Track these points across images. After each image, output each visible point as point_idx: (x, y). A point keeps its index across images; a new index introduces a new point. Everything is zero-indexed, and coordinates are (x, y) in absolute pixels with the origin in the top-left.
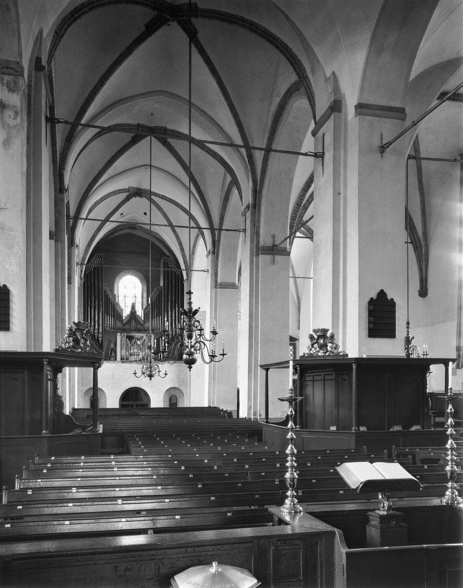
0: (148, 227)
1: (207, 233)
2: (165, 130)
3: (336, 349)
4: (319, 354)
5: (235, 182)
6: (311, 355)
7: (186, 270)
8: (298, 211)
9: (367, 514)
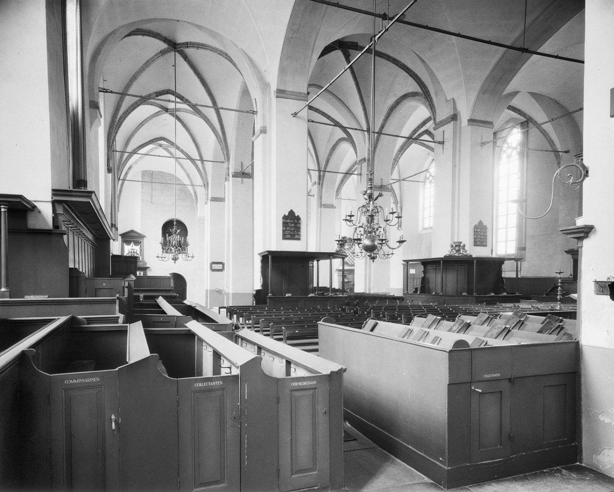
4: (456, 255)
6: (450, 256)
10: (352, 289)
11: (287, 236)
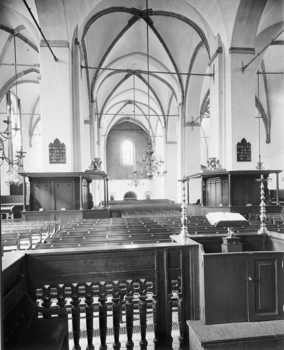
0: (133, 117)
1: (162, 118)
2: (141, 72)
3: (220, 167)
4: (212, 170)
5: (174, 93)
7: (153, 136)
8: (204, 105)
9: (222, 238)
10: (150, 198)
11: (241, 158)
